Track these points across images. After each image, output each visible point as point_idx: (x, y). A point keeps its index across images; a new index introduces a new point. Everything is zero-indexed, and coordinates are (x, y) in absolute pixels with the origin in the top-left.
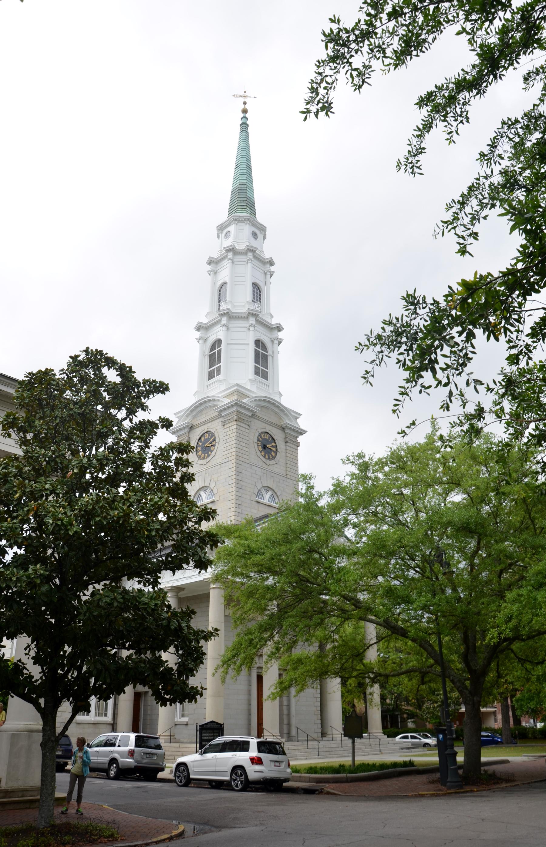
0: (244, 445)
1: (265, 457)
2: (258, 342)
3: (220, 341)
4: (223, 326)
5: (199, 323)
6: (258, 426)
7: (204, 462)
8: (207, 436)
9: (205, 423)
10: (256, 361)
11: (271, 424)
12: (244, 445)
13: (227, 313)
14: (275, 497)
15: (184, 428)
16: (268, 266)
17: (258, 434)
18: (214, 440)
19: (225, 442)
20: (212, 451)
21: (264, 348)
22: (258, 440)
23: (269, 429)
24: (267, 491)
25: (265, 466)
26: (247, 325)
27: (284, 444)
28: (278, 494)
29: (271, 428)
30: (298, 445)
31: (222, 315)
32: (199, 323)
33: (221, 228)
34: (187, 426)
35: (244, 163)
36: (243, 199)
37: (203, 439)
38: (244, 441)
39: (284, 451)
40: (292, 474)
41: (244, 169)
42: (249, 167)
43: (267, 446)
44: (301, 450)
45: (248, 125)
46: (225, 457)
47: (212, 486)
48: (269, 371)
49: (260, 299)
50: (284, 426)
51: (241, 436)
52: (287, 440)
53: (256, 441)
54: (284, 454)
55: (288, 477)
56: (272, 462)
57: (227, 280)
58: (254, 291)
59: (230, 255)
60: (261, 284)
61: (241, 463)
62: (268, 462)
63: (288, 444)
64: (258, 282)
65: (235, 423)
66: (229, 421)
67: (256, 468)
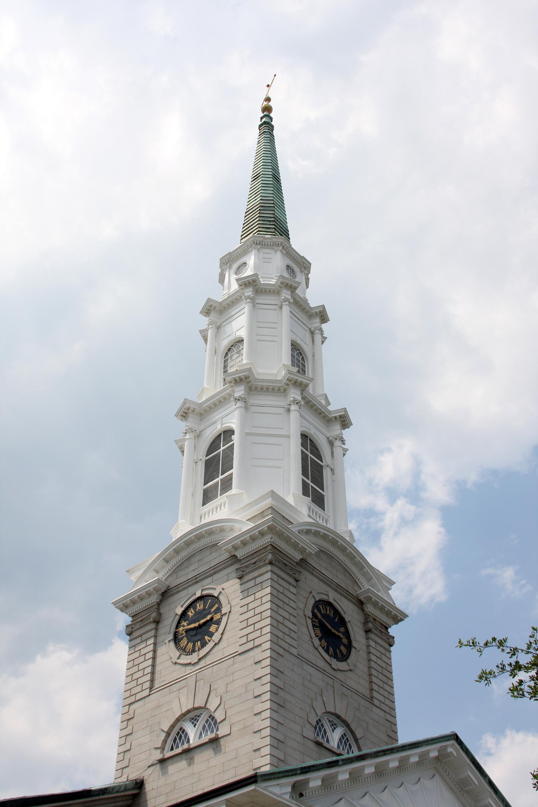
0: (287, 615)
1: (327, 651)
2: (306, 440)
3: (228, 433)
4: (237, 400)
5: (186, 401)
6: (314, 588)
7: (194, 658)
8: (200, 606)
9: (196, 580)
10: (305, 472)
11: (338, 588)
12: (287, 615)
13: (247, 377)
14: (352, 741)
15: (149, 594)
16: (318, 320)
17: (311, 602)
18: (219, 610)
19: (245, 609)
20: (211, 635)
21: (315, 450)
22: (314, 615)
23: (332, 596)
24: (334, 726)
25: (327, 668)
26: (284, 404)
27: (362, 633)
28: (359, 736)
29: (337, 596)
30: (390, 641)
31: (238, 381)
32: (186, 401)
33: (228, 261)
34: (156, 590)
35: (270, 172)
36: (269, 219)
37: (190, 614)
38: (286, 607)
39: (364, 648)
40: (382, 698)
41: (270, 180)
42: (276, 178)
43: (331, 631)
44: (397, 653)
45: (273, 127)
46: (244, 640)
47: (212, 706)
48: (328, 494)
49: (304, 371)
50: (362, 598)
51: (281, 596)
52: (370, 625)
53: (310, 615)
54: (363, 654)
55: (376, 702)
56: (342, 665)
57: (243, 333)
58: (293, 356)
59: (249, 292)
60: (307, 348)
61: (281, 651)
62: (334, 663)
63: (371, 635)
64: (299, 341)
65: (269, 567)
66: (256, 566)
67: (311, 670)
